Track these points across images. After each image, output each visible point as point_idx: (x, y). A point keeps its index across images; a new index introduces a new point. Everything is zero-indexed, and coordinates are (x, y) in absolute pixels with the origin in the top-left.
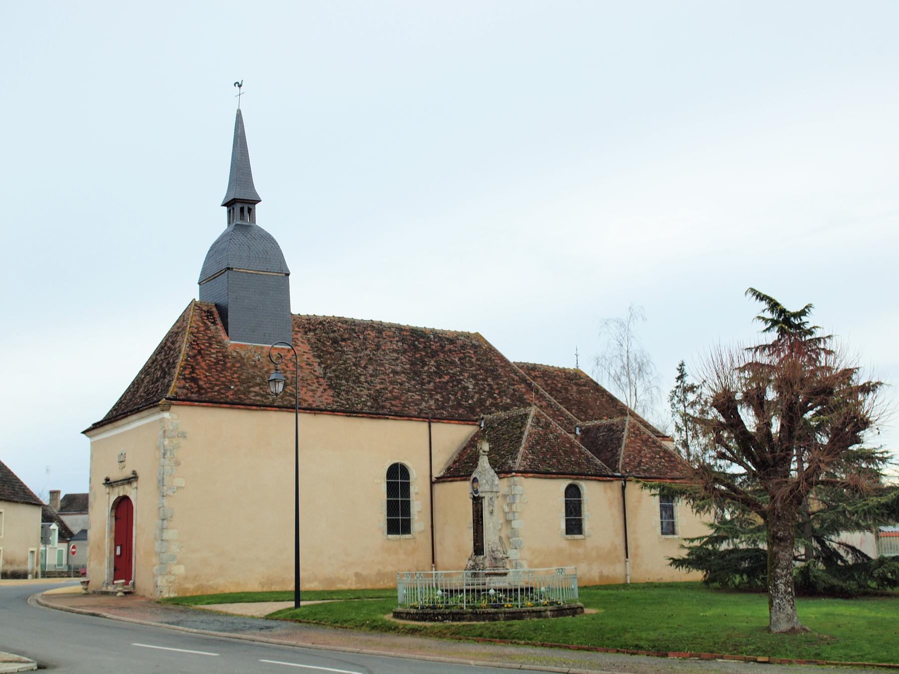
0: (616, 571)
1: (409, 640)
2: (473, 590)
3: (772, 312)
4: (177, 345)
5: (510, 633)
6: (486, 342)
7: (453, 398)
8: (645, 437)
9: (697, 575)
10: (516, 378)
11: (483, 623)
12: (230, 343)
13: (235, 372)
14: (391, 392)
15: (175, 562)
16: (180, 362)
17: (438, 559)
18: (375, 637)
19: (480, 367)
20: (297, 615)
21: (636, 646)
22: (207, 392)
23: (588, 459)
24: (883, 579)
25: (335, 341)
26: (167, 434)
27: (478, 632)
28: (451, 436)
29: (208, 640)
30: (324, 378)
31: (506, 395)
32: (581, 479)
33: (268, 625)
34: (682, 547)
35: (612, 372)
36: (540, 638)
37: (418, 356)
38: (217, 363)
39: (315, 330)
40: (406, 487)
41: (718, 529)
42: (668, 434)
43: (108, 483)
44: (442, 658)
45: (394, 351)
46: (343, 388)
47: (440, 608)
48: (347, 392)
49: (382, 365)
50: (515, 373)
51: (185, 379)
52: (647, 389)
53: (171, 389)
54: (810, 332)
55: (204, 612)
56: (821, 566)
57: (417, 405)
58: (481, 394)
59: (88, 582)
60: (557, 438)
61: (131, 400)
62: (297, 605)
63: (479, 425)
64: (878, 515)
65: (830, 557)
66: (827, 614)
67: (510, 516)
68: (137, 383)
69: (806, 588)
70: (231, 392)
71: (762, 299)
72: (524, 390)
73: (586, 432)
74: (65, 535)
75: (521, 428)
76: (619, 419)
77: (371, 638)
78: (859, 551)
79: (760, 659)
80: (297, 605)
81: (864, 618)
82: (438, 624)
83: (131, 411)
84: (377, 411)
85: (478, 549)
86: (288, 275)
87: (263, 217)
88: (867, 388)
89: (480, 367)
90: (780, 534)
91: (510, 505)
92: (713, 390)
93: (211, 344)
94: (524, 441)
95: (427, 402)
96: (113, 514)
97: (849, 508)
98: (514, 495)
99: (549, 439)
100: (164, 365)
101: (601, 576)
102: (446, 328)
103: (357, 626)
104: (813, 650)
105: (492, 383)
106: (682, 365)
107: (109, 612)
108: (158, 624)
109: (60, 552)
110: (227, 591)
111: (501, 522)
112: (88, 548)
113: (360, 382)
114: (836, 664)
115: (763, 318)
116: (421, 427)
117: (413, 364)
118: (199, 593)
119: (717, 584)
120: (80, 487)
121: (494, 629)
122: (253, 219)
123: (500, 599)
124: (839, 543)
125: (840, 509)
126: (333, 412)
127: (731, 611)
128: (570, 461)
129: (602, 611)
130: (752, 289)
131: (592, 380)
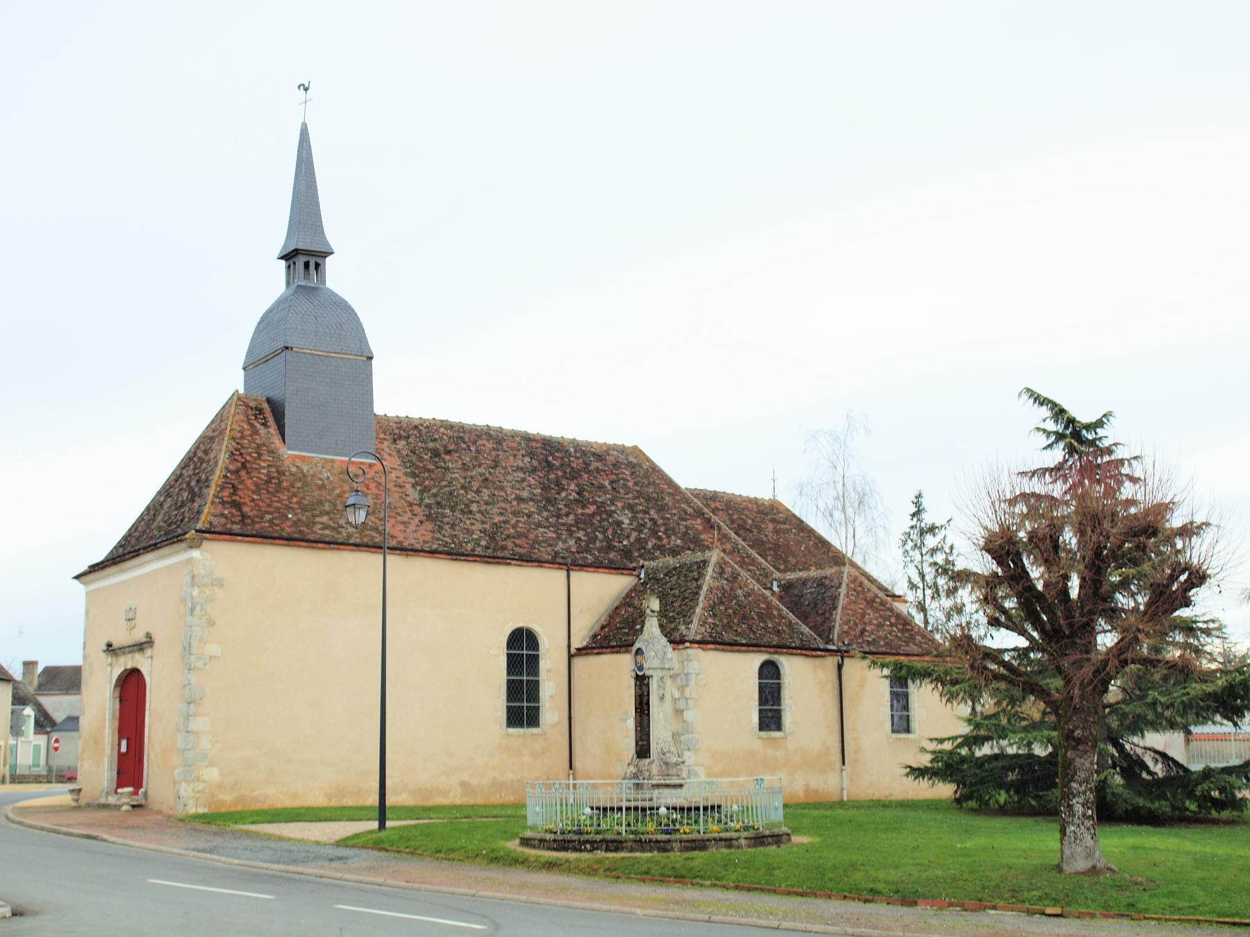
0: (829, 783)
1: (544, 878)
2: (636, 809)
3: (1056, 422)
4: (212, 455)
5: (690, 870)
6: (648, 460)
7: (600, 536)
8: (869, 596)
9: (945, 790)
10: (690, 510)
11: (649, 855)
12: (287, 453)
13: (295, 495)
14: (514, 527)
15: (206, 763)
16: (216, 478)
17: (577, 764)
18: (495, 873)
19: (639, 495)
20: (382, 841)
21: (871, 890)
22: (254, 522)
23: (790, 625)
24: (1206, 800)
25: (436, 453)
26: (197, 580)
27: (644, 868)
28: (600, 591)
29: (256, 875)
30: (420, 505)
31: (675, 534)
32: (782, 653)
33: (341, 855)
34: (923, 750)
35: (821, 505)
36: (733, 877)
37: (552, 476)
38: (269, 481)
39: (407, 438)
40: (534, 661)
41: (977, 726)
42: (897, 593)
43: (110, 648)
44: (596, 905)
45: (519, 469)
46: (446, 520)
48: (453, 526)
49: (502, 489)
51: (223, 503)
52: (869, 530)
53: (203, 517)
54: (1109, 451)
55: (248, 834)
56: (1118, 780)
57: (550, 545)
58: (640, 532)
59: (80, 790)
60: (747, 595)
61: (144, 532)
62: (382, 826)
63: (638, 576)
64: (1202, 708)
65: (1131, 766)
66: (1135, 848)
67: (681, 705)
68: (153, 509)
69: (1108, 812)
70: (289, 523)
71: (1041, 404)
72: (700, 528)
73: (787, 587)
74: (45, 723)
75: (697, 580)
76: (835, 569)
77: (491, 874)
78: (1173, 760)
79: (1049, 911)
80: (382, 826)
81: (1188, 853)
82: (585, 855)
83: (145, 548)
84: (496, 551)
85: (643, 751)
86: (371, 358)
88: (1188, 531)
90: (1078, 733)
91: (681, 688)
92: (986, 528)
93: (260, 455)
94: (701, 598)
95: (565, 542)
96: (117, 694)
97: (1163, 699)
99: (736, 597)
100: (193, 483)
101: (807, 791)
102: (592, 439)
103: (468, 858)
104: (1124, 898)
105: (655, 516)
106: (919, 496)
107: (110, 834)
108: (182, 852)
109: (37, 748)
110: (279, 805)
112: (80, 743)
113: (471, 512)
114: (1158, 919)
115: (1044, 431)
116: (553, 578)
117: (545, 488)
118: (239, 808)
119: (972, 804)
120: (67, 655)
121: (666, 865)
122: (322, 280)
123: (674, 822)
124: (1145, 748)
125: (1149, 699)
126: (433, 553)
127: (1001, 841)
128: (766, 628)
129: (817, 839)
130: (1028, 390)
131: (794, 516)
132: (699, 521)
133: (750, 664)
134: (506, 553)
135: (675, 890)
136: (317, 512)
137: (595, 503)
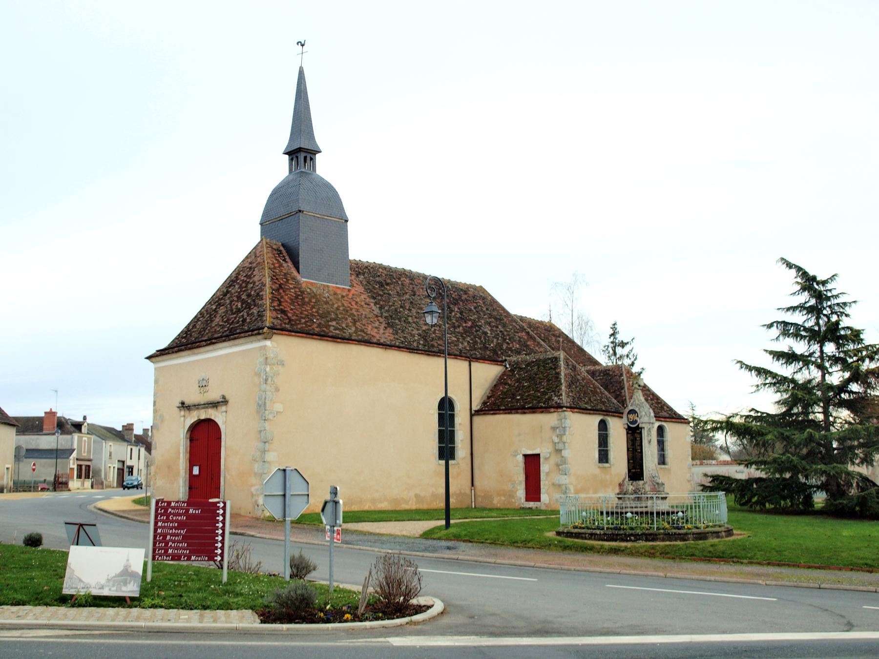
17: (476, 483)
25: (381, 285)
28: (486, 374)
38: (297, 297)
39: (364, 274)
43: (183, 406)
47: (624, 529)
50: (516, 322)
51: (275, 310)
60: (583, 379)
63: (505, 366)
67: (560, 446)
69: (838, 511)
70: (315, 325)
71: (791, 268)
80: (448, 525)
84: (428, 347)
86: (347, 221)
87: (324, 167)
89: (491, 316)
91: (560, 436)
93: (288, 280)
94: (563, 381)
95: (462, 343)
96: (188, 436)
98: (564, 428)
111: (550, 451)
126: (399, 348)
130: (782, 259)
132: (524, 334)
133: (594, 420)
134: (435, 349)
135: (730, 567)
136: (328, 319)
137: (470, 320)
